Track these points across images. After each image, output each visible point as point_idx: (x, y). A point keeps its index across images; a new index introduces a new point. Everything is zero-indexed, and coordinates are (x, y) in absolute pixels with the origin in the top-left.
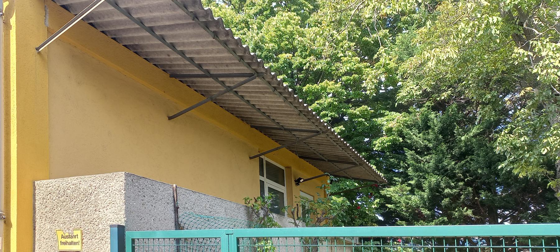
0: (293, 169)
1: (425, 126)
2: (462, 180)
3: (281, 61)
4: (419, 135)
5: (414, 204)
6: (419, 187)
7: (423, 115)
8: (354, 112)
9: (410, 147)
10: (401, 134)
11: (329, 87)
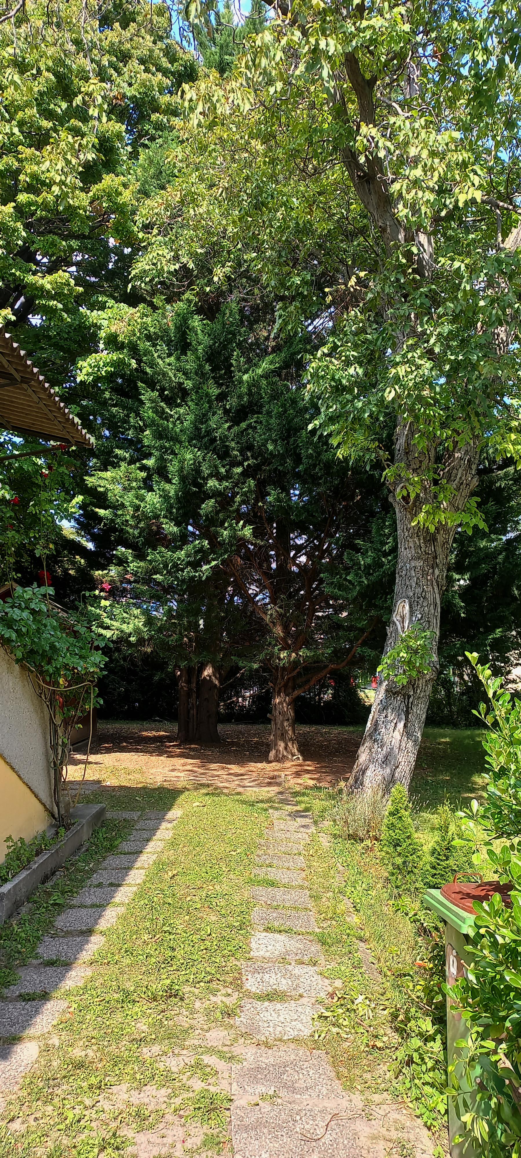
2: (240, 464)
4: (167, 360)
5: (148, 509)
6: (162, 472)
7: (179, 315)
8: (41, 281)
9: (151, 384)
10: (134, 350)
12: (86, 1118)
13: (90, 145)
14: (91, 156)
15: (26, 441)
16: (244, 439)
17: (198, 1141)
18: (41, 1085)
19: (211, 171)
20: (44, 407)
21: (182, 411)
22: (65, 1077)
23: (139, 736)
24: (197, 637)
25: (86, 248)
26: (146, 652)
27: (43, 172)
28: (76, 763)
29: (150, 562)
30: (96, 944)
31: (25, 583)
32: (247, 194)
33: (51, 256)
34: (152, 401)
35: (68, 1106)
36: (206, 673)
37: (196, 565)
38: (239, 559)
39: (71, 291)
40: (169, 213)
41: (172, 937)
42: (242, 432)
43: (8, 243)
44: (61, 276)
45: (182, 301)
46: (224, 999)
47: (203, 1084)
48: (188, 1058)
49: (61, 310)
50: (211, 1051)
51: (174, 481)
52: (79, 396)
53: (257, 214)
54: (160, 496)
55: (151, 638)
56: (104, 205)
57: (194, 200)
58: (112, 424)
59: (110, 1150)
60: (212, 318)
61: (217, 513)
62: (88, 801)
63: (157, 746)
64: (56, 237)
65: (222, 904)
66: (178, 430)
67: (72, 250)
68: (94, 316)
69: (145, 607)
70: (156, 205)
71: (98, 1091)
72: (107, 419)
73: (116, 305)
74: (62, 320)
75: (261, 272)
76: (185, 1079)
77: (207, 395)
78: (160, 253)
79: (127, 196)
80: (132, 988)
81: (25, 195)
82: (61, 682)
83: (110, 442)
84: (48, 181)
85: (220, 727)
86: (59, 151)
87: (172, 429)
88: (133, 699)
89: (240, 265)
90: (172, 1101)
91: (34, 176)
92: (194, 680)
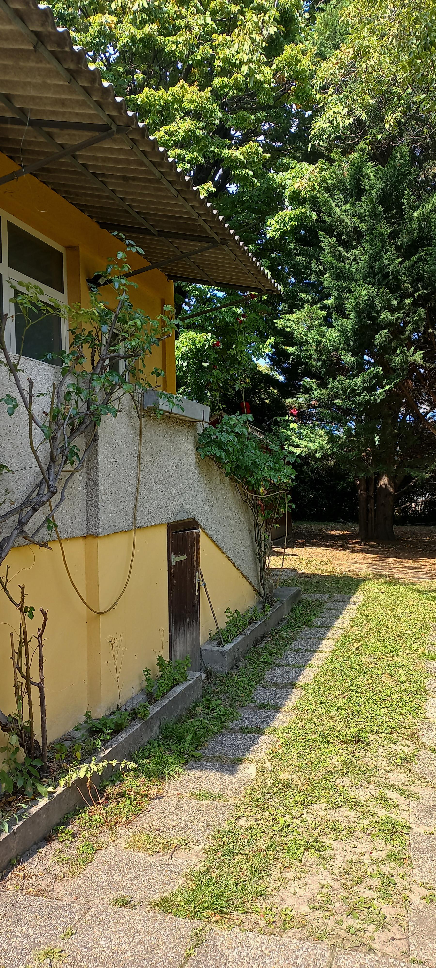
0: (84, 252)
1: (356, 190)
2: (411, 295)
3: (93, 31)
4: (344, 208)
5: (329, 343)
6: (340, 310)
7: (353, 165)
9: (329, 231)
11: (187, 96)
12: (294, 825)
13: (272, 20)
14: (272, 30)
15: (228, 294)
16: (415, 272)
17: (383, 854)
18: (259, 796)
19: (382, 22)
20: (239, 263)
21: (356, 252)
22: (277, 793)
23: (326, 534)
24: (373, 452)
25: (272, 117)
26: (330, 466)
27: (233, 55)
28: (277, 554)
29: (332, 389)
30: (296, 696)
31: (230, 411)
32: (417, 37)
33: (243, 130)
34: (331, 247)
35: (280, 814)
36: (382, 482)
37: (371, 389)
38: (410, 382)
39: (259, 159)
40: (343, 71)
41: (358, 695)
42: (413, 266)
43: (207, 124)
44: (252, 146)
45: (357, 151)
46: (403, 748)
47: (386, 813)
48: (372, 791)
49: (252, 176)
50: (393, 788)
51: (351, 317)
52: (269, 250)
53: (426, 54)
54: (339, 331)
55: (334, 453)
56: (286, 75)
57: (365, 54)
58: (298, 272)
59: (312, 851)
60: (383, 163)
61: (390, 342)
62: (287, 583)
63: (342, 543)
64: (245, 113)
65: (400, 672)
66: (354, 270)
67: (259, 121)
68: (278, 177)
69: (328, 427)
70: (331, 65)
71: (302, 807)
72: (293, 267)
73: (298, 165)
74: (253, 184)
75: (430, 112)
76: (371, 807)
77: (381, 235)
78: (336, 110)
79: (305, 62)
80: (327, 732)
81: (220, 79)
82: (261, 491)
83: (296, 287)
84: (237, 62)
85: (395, 528)
86: (245, 32)
87: (349, 269)
88: (319, 503)
89: (409, 109)
90: (361, 822)
91: (226, 60)
92: (372, 488)
